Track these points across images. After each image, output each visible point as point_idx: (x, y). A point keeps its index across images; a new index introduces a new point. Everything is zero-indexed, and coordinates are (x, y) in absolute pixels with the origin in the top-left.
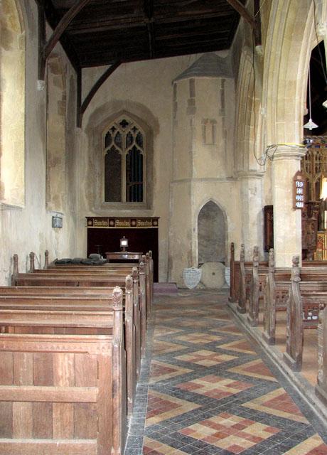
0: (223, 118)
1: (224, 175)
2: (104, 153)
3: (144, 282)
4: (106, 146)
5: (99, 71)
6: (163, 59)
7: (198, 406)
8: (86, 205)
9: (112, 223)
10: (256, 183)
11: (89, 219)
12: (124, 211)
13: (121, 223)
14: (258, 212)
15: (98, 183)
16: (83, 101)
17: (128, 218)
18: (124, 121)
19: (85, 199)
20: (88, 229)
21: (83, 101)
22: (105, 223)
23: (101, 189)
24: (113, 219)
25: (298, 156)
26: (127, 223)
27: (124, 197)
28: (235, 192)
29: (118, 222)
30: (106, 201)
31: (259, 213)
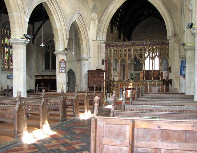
0: (76, 38)
1: (76, 60)
2: (44, 53)
3: (195, 85)
4: (52, 49)
5: (39, 23)
6: (32, 11)
7: (73, 145)
8: (36, 71)
9: (50, 77)
10: (86, 62)
11: (36, 76)
12: (48, 73)
13: (46, 77)
14: (85, 73)
15: (41, 63)
16: (35, 33)
17: (48, 75)
18: (51, 40)
19: (35, 69)
20: (36, 79)
21: (35, 33)
22: (41, 77)
23: (42, 65)
24: (43, 76)
25: (24, 43)
26: (48, 77)
27: (50, 68)
28: (78, 66)
29: (45, 77)
30: (52, 69)
31: (86, 74)
